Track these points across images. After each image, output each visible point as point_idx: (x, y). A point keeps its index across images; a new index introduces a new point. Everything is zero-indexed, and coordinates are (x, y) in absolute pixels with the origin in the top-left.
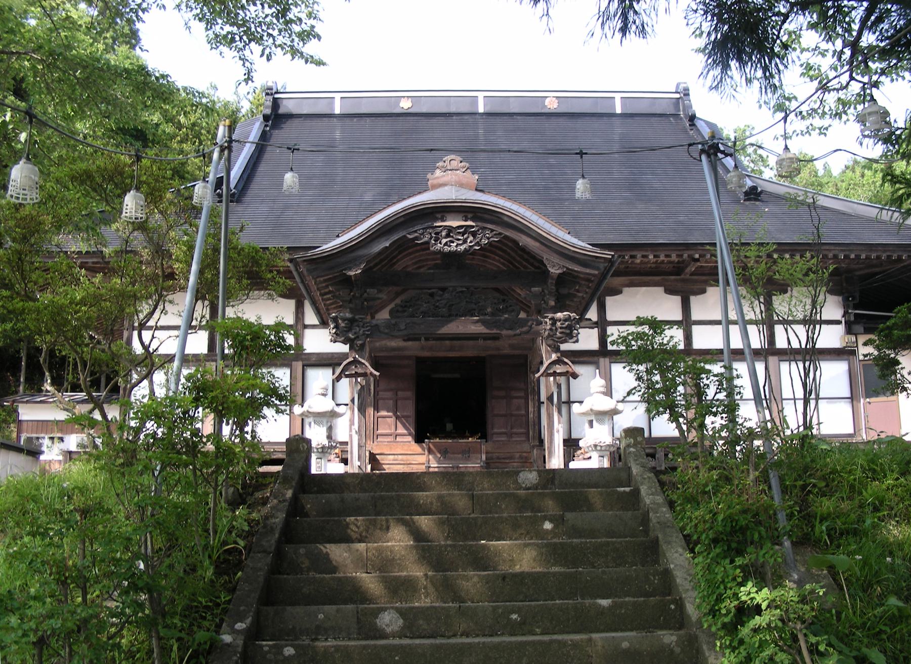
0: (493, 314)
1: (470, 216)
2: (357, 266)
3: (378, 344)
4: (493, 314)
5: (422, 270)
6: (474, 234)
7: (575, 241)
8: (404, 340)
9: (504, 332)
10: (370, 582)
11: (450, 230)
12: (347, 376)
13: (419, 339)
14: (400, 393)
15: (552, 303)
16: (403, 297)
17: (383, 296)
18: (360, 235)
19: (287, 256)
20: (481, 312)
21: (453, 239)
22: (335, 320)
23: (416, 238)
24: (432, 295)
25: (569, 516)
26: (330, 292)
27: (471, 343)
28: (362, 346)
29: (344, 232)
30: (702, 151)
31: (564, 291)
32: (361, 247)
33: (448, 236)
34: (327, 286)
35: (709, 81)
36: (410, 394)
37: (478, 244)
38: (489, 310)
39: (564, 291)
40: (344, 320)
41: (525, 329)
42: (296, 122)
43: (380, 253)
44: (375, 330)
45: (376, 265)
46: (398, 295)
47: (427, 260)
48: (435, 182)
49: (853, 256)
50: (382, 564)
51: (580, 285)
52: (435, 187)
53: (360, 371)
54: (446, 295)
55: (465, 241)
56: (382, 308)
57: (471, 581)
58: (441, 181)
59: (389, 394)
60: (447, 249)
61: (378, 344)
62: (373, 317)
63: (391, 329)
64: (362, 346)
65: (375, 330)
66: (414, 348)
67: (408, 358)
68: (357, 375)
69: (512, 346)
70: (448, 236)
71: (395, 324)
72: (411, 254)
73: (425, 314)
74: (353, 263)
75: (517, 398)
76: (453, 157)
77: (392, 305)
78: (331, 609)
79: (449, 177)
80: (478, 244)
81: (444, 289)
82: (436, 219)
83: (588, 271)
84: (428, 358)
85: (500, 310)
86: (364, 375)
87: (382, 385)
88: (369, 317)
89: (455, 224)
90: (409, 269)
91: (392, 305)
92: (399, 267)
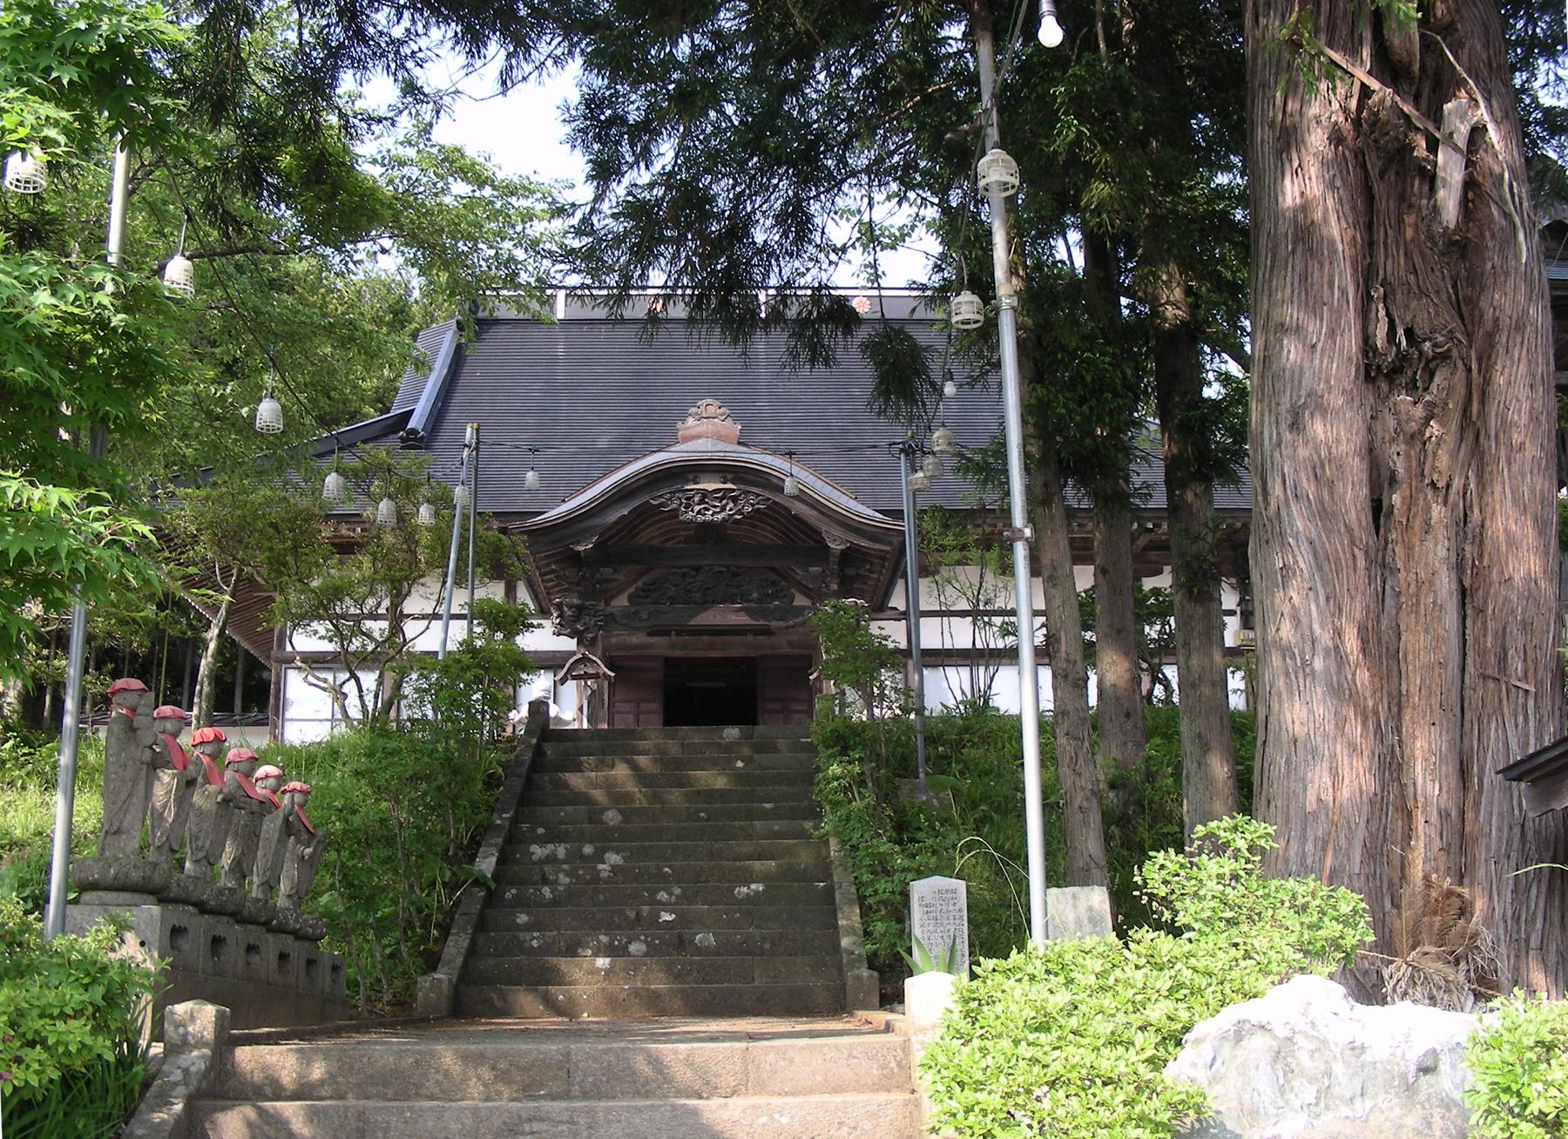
0: (759, 601)
1: (729, 476)
2: (587, 539)
3: (613, 640)
4: (759, 601)
5: (669, 544)
6: (735, 500)
7: (861, 509)
8: (649, 635)
9: (774, 624)
10: (599, 795)
11: (705, 494)
12: (574, 678)
13: (666, 633)
14: (643, 705)
15: (835, 587)
16: (645, 578)
17: (620, 577)
18: (591, 501)
19: (496, 525)
20: (744, 598)
21: (707, 505)
22: (559, 607)
23: (662, 505)
24: (684, 575)
25: (756, 756)
26: (553, 571)
27: (737, 639)
28: (594, 640)
29: (572, 496)
30: (902, 450)
31: (850, 572)
32: (593, 516)
33: (701, 502)
34: (549, 565)
35: (876, 407)
36: (656, 706)
37: (739, 512)
38: (755, 595)
39: (850, 572)
40: (570, 607)
41: (800, 619)
42: (503, 328)
43: (616, 523)
44: (610, 621)
45: (611, 538)
46: (641, 574)
47: (678, 530)
48: (687, 433)
49: (1239, 525)
50: (609, 785)
51: (872, 564)
52: (687, 439)
53: (591, 671)
54: (701, 577)
55: (723, 509)
56: (620, 592)
57: (675, 796)
58: (694, 432)
59: (628, 707)
60: (700, 518)
61: (613, 640)
62: (607, 604)
63: (629, 620)
64: (594, 640)
65: (610, 621)
66: (661, 646)
67: (655, 658)
68: (586, 676)
69: (791, 644)
70: (701, 502)
71: (635, 613)
72: (655, 523)
73: (673, 600)
74: (582, 536)
75: (797, 712)
76: (709, 401)
77: (632, 589)
78: (570, 809)
79: (705, 426)
80: (739, 512)
81: (697, 569)
82: (687, 481)
83: (877, 546)
84: (680, 658)
85: (767, 595)
86: (595, 676)
87: (619, 696)
88: (602, 604)
89: (711, 486)
90: (653, 543)
91: (632, 589)
92: (642, 539)
